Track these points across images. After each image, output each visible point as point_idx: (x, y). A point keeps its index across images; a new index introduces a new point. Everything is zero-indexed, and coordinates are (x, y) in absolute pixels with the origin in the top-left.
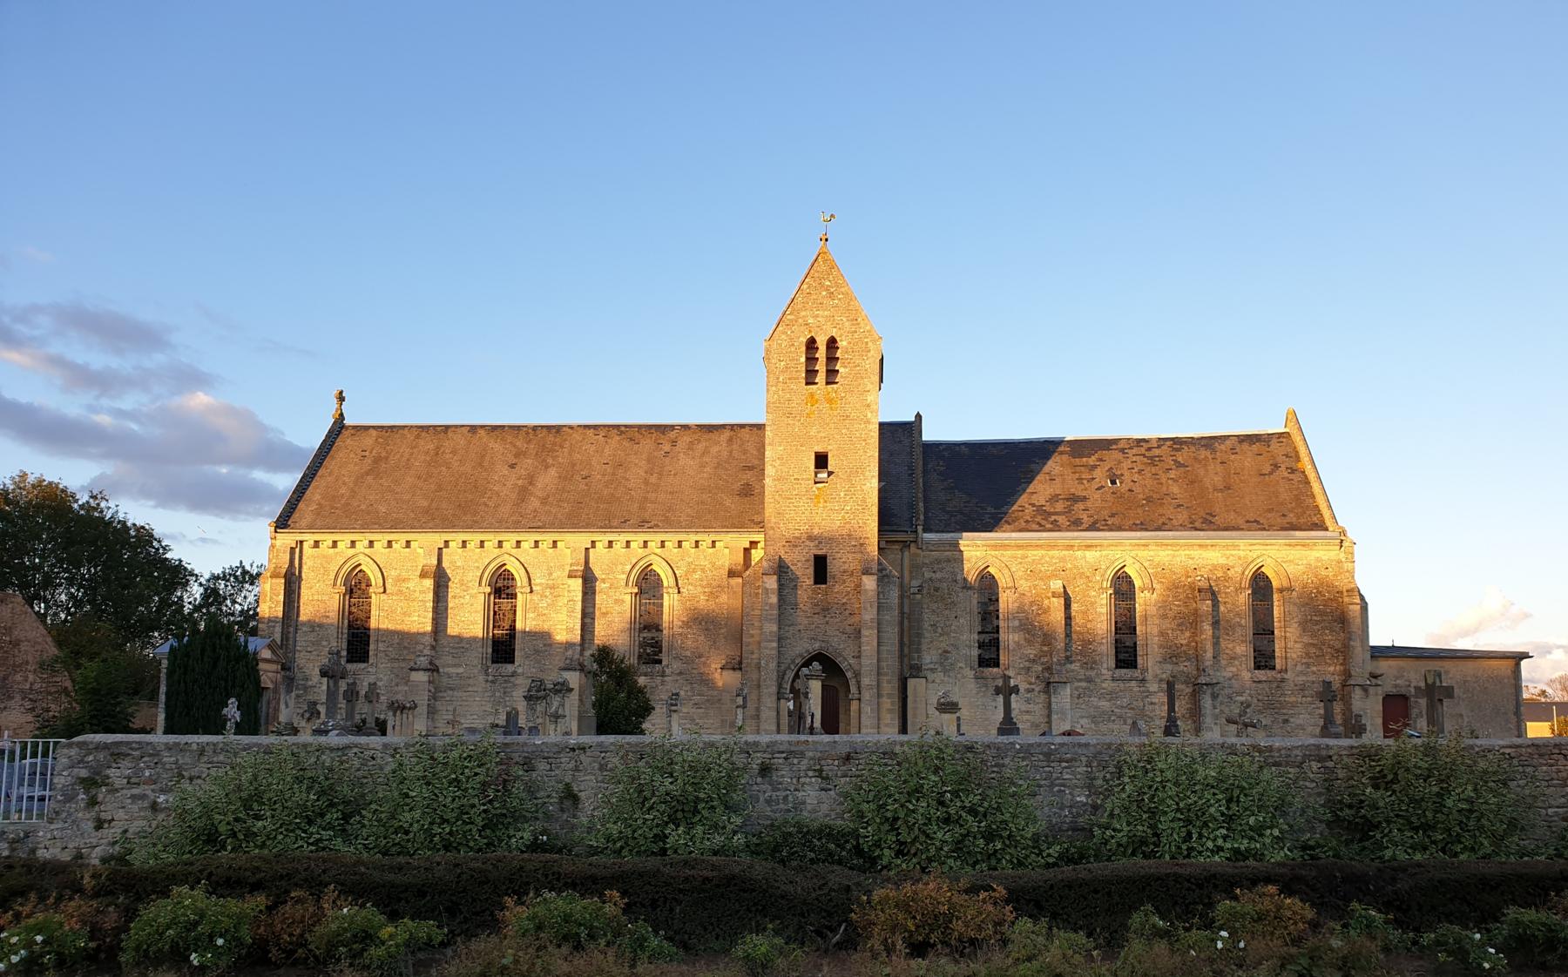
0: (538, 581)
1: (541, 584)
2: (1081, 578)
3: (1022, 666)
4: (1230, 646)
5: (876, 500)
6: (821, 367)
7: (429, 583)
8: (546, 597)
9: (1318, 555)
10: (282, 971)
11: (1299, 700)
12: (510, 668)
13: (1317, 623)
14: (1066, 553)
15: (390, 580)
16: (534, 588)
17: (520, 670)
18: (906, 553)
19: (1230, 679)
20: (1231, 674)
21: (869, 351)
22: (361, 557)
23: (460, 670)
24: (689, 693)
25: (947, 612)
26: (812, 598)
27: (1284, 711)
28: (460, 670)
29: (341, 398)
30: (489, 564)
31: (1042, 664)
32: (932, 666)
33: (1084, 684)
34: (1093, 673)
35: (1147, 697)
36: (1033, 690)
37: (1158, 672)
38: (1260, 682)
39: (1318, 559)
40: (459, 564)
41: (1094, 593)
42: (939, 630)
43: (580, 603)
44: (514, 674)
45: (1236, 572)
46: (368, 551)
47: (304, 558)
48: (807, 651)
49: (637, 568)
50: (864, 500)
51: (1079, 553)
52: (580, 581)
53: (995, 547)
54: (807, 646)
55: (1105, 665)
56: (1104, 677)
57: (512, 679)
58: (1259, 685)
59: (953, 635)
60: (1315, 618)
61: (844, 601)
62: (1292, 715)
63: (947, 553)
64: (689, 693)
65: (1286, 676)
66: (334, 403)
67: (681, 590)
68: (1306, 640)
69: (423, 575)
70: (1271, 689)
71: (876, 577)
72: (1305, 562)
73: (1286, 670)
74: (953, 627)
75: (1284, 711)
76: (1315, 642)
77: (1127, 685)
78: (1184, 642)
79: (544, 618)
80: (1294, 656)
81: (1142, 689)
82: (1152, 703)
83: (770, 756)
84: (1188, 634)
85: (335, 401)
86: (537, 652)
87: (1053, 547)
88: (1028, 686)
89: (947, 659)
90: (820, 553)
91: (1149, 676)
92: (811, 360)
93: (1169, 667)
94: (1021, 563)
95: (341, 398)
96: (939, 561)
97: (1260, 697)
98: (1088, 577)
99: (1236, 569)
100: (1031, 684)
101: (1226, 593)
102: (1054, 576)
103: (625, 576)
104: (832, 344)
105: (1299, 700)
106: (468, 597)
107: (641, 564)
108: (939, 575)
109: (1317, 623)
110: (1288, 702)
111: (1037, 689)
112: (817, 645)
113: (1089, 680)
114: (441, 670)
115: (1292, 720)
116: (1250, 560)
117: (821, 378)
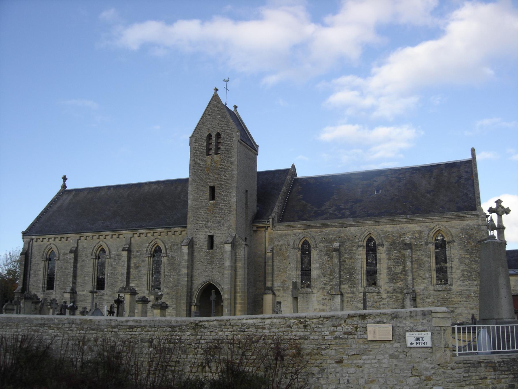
0: (113, 253)
1: (114, 254)
2: (349, 241)
3: (320, 287)
4: (423, 273)
5: (497, 220)
6: (213, 147)
7: (72, 255)
8: (116, 260)
9: (467, 223)
10: (465, 388)
11: (459, 300)
12: (102, 291)
13: (467, 258)
14: (341, 228)
15: (61, 255)
16: (112, 256)
17: (105, 293)
18: (267, 233)
19: (423, 290)
20: (423, 288)
21: (233, 138)
22: (52, 245)
23: (84, 293)
24: (171, 304)
25: (285, 261)
26: (207, 256)
27: (452, 306)
28: (84, 293)
29: (65, 179)
30: (95, 246)
31: (330, 285)
32: (278, 288)
33: (350, 295)
34: (354, 290)
35: (381, 301)
36: (326, 299)
37: (387, 288)
38: (438, 291)
39: (467, 225)
40: (85, 246)
41: (355, 248)
42: (282, 270)
43: (126, 262)
44: (103, 295)
45: (425, 234)
46: (54, 242)
47: (33, 246)
48: (204, 282)
49: (151, 245)
50: (230, 208)
51: (347, 229)
52: (127, 252)
53: (307, 228)
54: (204, 280)
55: (360, 285)
56: (360, 291)
57: (103, 297)
58: (438, 293)
59: (288, 272)
60: (466, 256)
61: (221, 257)
62: (456, 308)
63: (285, 232)
64: (171, 304)
65: (452, 288)
66: (62, 181)
67: (168, 255)
68: (462, 267)
69: (71, 252)
70: (444, 294)
71: (231, 245)
72: (461, 227)
73: (452, 284)
74: (288, 269)
75: (452, 306)
76: (467, 268)
77: (372, 295)
78: (399, 272)
79: (115, 269)
80: (456, 277)
81: (378, 297)
82: (384, 304)
83: (277, 330)
84: (401, 267)
85: (62, 180)
86: (112, 284)
87: (334, 227)
88: (324, 297)
89: (285, 284)
90: (211, 234)
91: (382, 289)
92: (209, 144)
93: (393, 285)
94: (319, 235)
95: (65, 179)
96: (281, 236)
97: (439, 299)
98: (351, 240)
99: (425, 233)
100: (325, 296)
101: (420, 245)
102: (335, 240)
103: (146, 249)
104: (218, 135)
105: (459, 300)
106: (87, 261)
107: (152, 243)
108: (281, 243)
109: (467, 258)
110: (453, 301)
111: (328, 298)
112: (208, 278)
113: (353, 293)
114: (77, 293)
115: (455, 311)
116: (432, 227)
117: (212, 152)
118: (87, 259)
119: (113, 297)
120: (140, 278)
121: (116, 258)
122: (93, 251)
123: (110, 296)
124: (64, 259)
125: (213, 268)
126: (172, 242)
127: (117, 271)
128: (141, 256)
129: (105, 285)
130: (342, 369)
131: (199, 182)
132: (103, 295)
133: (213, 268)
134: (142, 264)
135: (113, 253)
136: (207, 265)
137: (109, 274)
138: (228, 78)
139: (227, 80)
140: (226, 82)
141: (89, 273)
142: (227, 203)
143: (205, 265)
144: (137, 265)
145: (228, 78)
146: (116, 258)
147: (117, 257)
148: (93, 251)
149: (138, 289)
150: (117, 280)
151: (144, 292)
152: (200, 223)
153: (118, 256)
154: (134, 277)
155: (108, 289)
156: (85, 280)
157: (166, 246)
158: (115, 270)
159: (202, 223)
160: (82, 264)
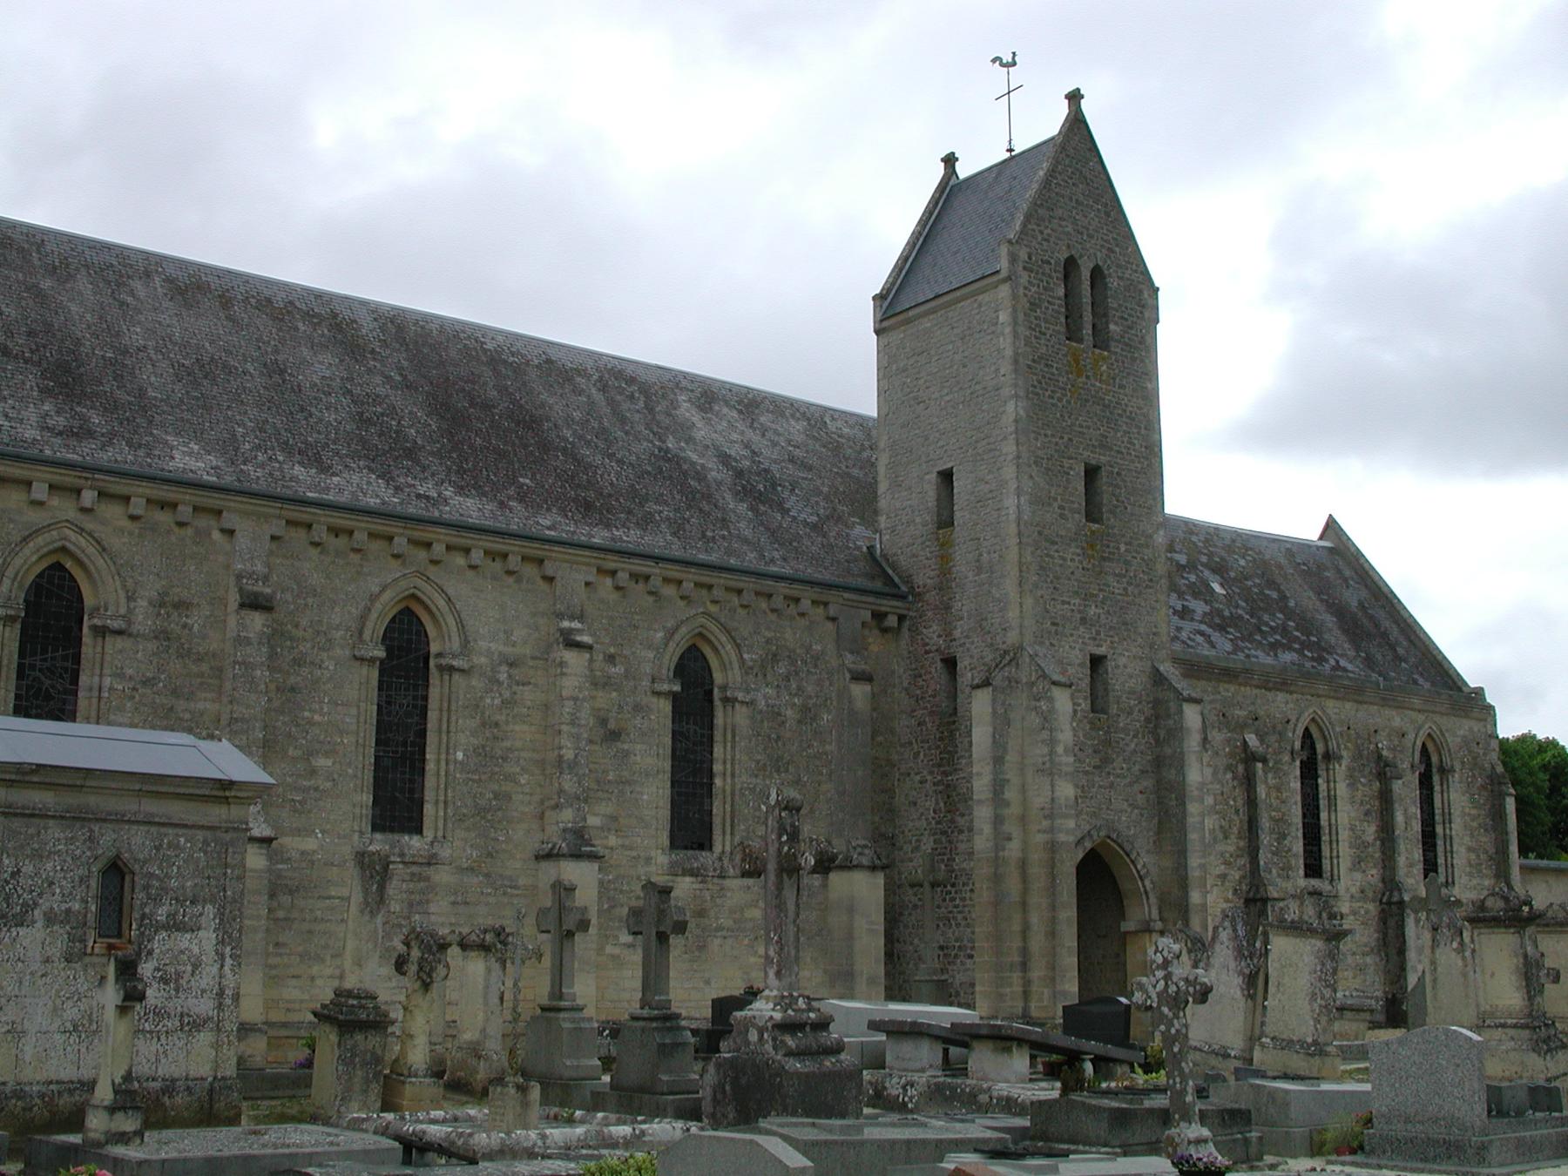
1: (489, 653)
8: (500, 683)
23: (310, 844)
28: (310, 844)
57: (430, 871)
118: (324, 655)
119: (487, 875)
120: (628, 789)
121: (503, 677)
122: (363, 618)
123: (472, 869)
124: (162, 635)
125: (1112, 785)
126: (768, 641)
127: (507, 744)
128: (632, 683)
129: (428, 809)
130: (417, 1148)
131: (1053, 436)
132: (429, 864)
133: (1112, 785)
134: (638, 721)
135: (483, 644)
136: (1093, 773)
137: (460, 755)
138: (1014, 53)
139: (1007, 58)
140: (1002, 65)
141: (341, 733)
142: (1139, 545)
143: (1086, 773)
144: (612, 725)
145: (1014, 53)
146: (503, 677)
147: (504, 668)
148: (363, 618)
149: (620, 842)
150: (507, 787)
151: (648, 860)
152: (1063, 603)
153: (511, 665)
154: (598, 782)
155: (460, 833)
156: (313, 772)
157: (746, 656)
158: (496, 738)
159: (1069, 603)
160: (292, 680)
